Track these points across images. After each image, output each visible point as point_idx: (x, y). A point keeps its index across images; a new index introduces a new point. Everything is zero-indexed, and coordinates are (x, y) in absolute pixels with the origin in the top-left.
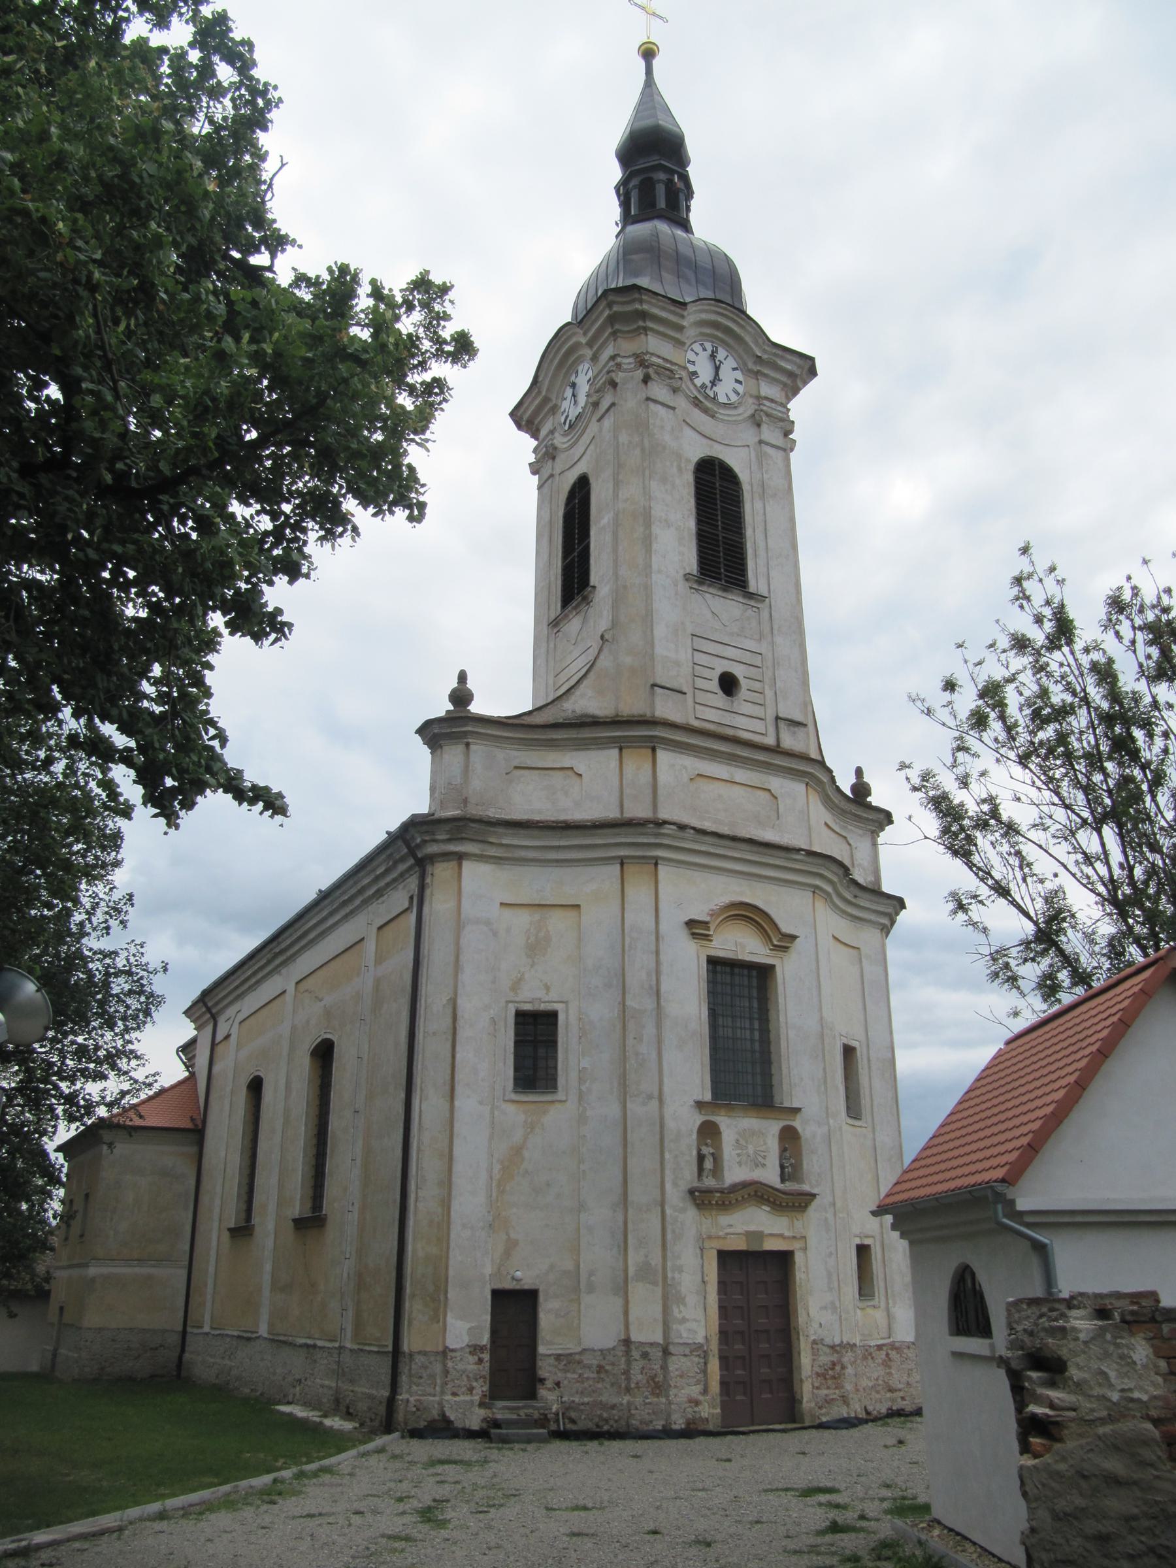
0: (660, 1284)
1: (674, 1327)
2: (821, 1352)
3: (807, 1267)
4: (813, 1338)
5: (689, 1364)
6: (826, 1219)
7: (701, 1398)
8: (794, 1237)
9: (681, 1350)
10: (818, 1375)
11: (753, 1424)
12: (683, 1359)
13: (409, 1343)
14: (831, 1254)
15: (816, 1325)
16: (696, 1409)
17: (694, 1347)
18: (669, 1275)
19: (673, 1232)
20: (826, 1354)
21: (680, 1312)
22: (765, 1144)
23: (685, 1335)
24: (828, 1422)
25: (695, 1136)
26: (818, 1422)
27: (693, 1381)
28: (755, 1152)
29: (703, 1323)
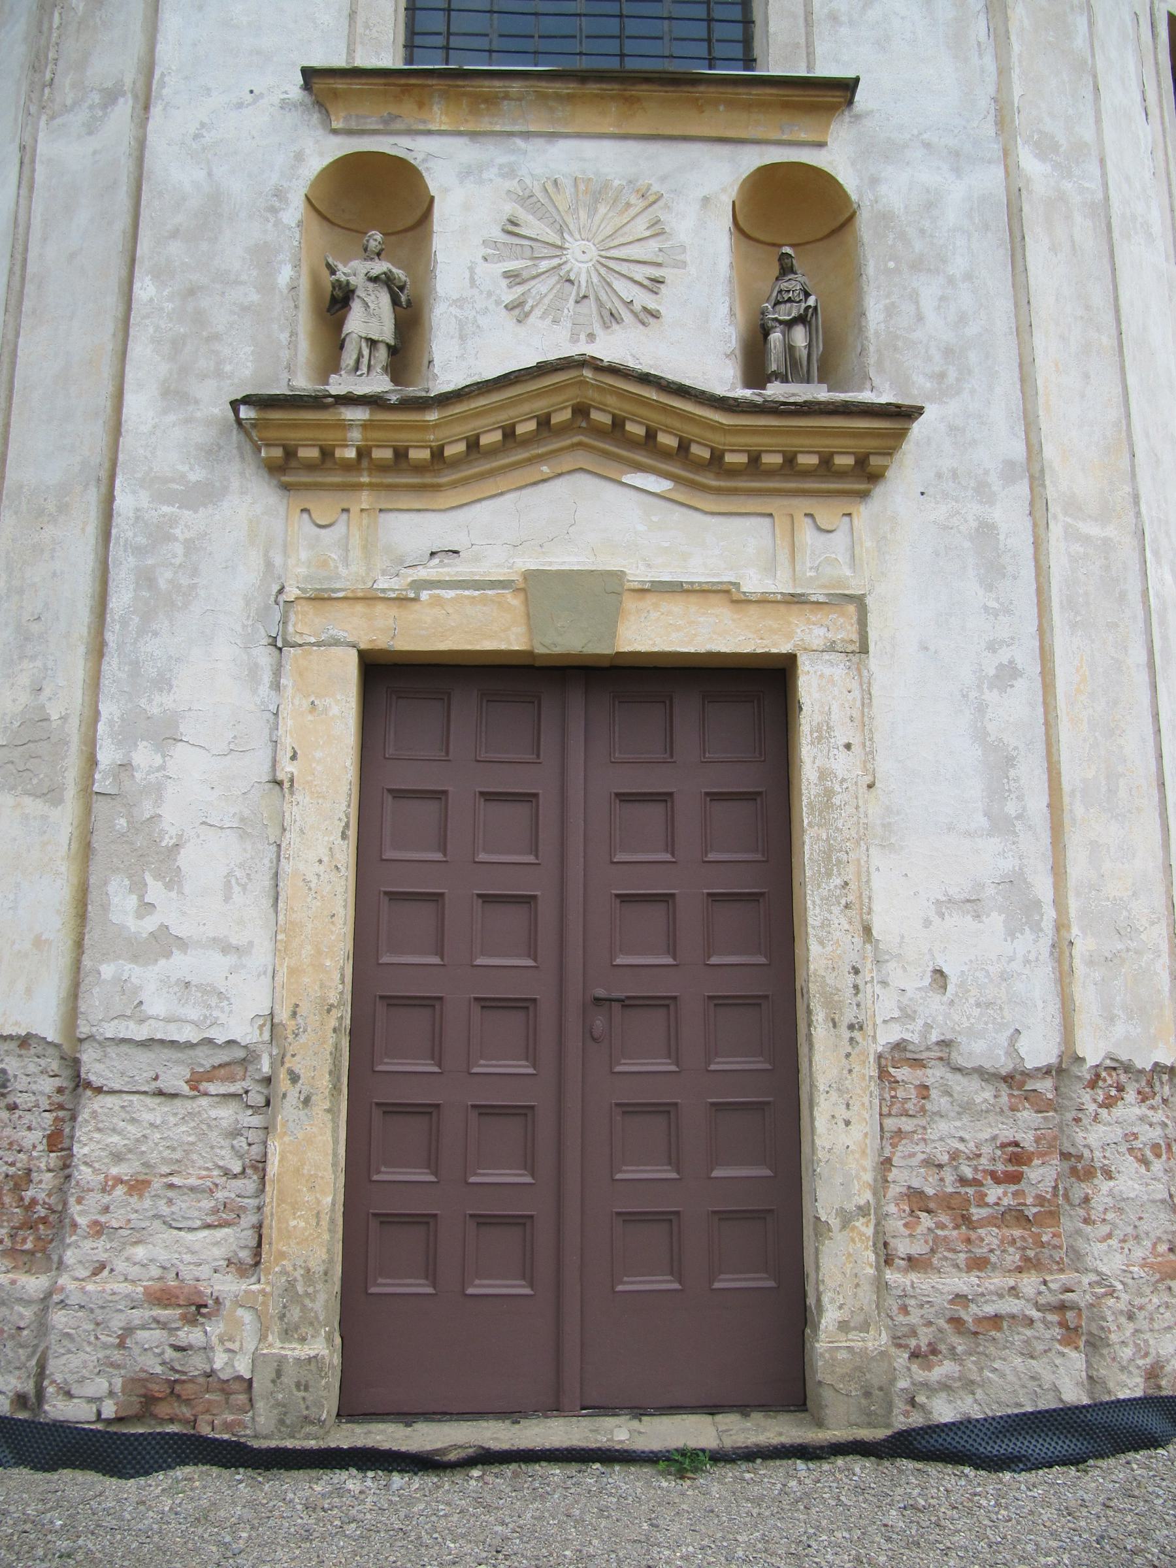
0: (71, 792)
1: (107, 971)
2: (938, 1101)
3: (864, 721)
4: (887, 1036)
5: (183, 1132)
6: (986, 531)
7: (228, 1286)
8: (795, 600)
9: (141, 1066)
10: (917, 1200)
11: (555, 1407)
12: (152, 1112)
13: (162, 1015)
14: (1007, 674)
15: (914, 981)
16: (191, 1336)
17: (207, 1060)
18: (107, 756)
19: (146, 579)
20: (966, 1108)
21: (147, 908)
22: (658, 230)
23: (157, 1006)
24: (965, 1425)
25: (294, 211)
26: (903, 1420)
27: (199, 1208)
28: (604, 263)
29: (261, 956)
